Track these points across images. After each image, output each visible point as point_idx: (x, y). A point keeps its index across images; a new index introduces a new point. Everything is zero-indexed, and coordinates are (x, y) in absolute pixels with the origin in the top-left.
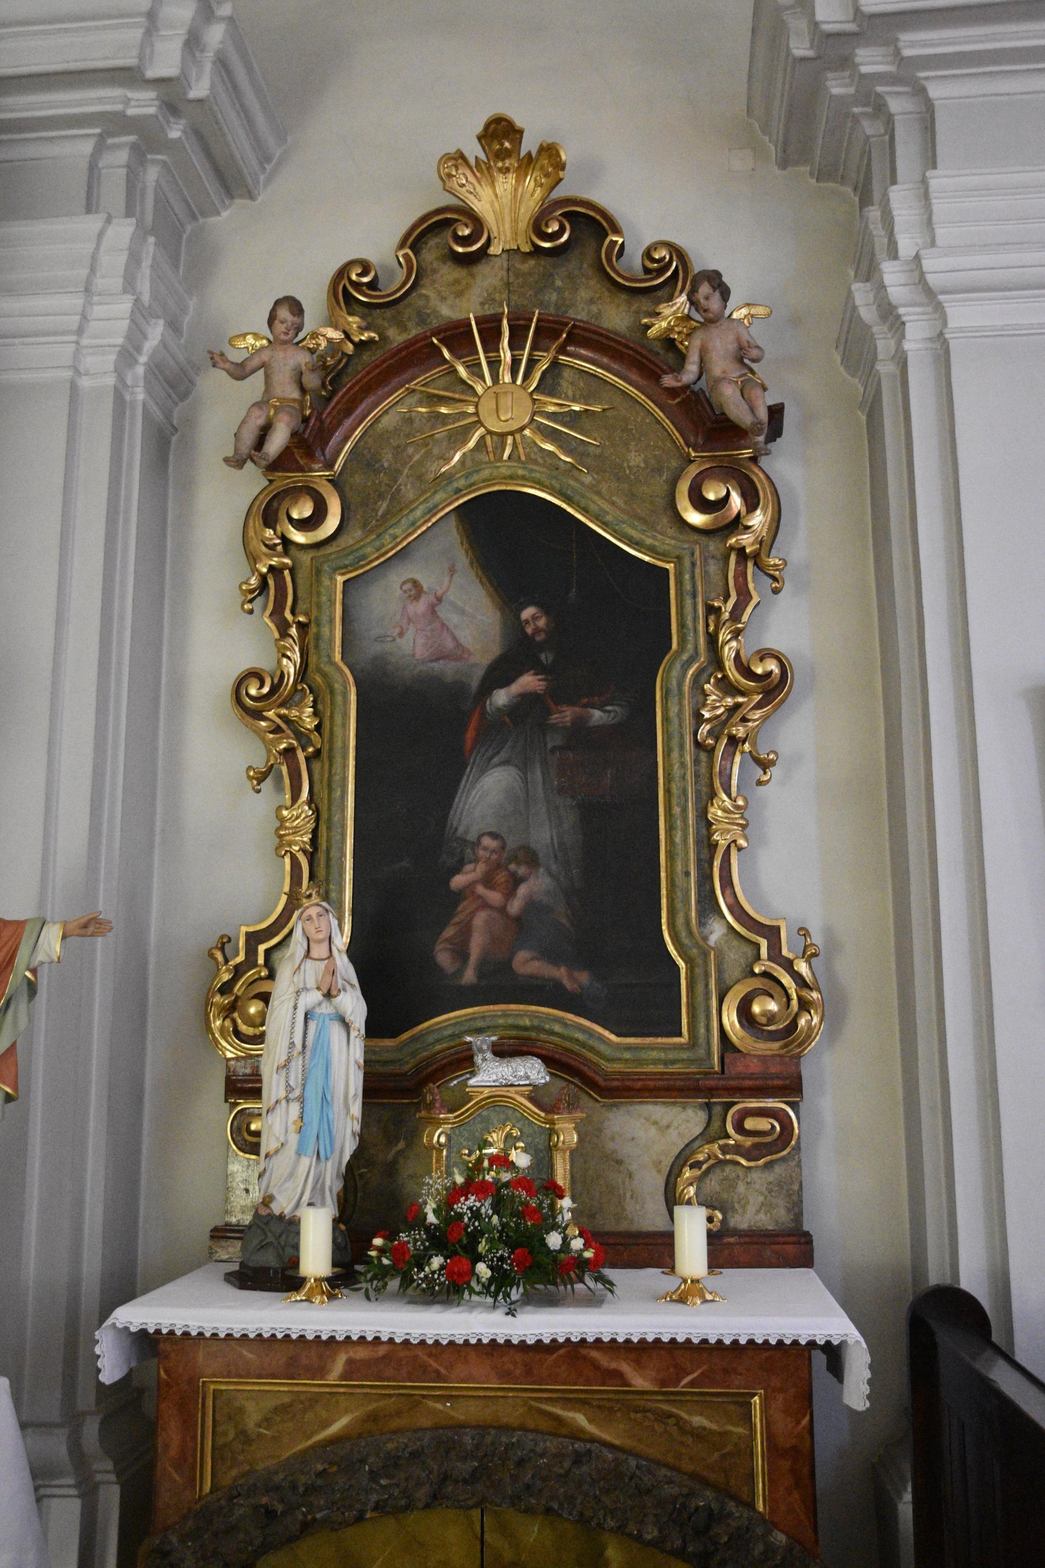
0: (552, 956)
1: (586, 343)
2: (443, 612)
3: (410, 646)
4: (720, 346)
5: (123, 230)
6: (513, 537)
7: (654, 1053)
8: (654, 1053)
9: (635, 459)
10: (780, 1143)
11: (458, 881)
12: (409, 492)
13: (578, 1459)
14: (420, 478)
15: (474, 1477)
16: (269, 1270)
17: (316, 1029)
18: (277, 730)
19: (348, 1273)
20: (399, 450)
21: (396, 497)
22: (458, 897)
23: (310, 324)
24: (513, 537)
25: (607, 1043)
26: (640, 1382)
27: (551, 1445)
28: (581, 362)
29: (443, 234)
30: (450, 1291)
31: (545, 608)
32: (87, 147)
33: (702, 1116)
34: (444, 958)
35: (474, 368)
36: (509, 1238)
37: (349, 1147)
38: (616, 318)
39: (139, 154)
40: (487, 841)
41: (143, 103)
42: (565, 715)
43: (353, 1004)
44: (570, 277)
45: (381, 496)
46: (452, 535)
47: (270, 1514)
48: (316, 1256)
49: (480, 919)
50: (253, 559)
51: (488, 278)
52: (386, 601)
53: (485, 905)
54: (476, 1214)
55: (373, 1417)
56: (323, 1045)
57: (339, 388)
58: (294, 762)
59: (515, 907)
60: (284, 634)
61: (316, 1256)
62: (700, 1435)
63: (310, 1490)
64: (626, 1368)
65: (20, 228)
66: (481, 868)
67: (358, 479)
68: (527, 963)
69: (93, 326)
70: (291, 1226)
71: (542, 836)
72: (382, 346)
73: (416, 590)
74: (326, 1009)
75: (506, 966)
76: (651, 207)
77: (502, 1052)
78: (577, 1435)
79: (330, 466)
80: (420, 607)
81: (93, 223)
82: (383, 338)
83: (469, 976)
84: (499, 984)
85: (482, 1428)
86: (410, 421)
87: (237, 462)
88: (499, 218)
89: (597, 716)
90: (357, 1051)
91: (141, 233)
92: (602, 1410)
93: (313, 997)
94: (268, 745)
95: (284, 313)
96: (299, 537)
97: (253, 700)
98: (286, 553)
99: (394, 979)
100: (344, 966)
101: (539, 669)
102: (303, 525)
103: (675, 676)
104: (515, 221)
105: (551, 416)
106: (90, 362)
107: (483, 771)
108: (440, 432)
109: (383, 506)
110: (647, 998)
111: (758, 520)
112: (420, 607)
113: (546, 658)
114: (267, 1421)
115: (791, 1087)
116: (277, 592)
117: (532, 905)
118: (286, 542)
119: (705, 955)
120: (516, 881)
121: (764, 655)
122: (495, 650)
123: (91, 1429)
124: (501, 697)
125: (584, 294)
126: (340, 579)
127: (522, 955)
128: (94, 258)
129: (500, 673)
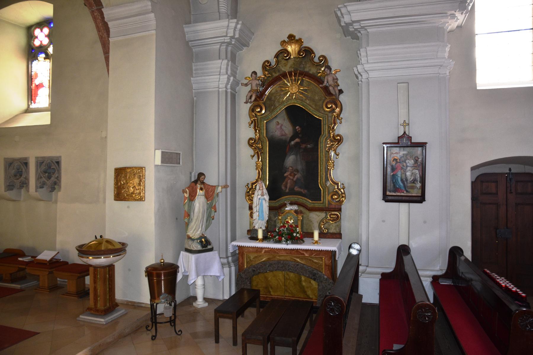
0: (300, 187)
1: (308, 76)
2: (283, 127)
3: (277, 134)
4: (330, 79)
5: (225, 62)
6: (295, 113)
7: (317, 204)
8: (317, 204)
9: (317, 98)
10: (337, 219)
11: (285, 175)
12: (277, 105)
14: (279, 102)
15: (282, 267)
16: (254, 238)
17: (262, 200)
18: (255, 149)
19: (265, 238)
20: (275, 97)
21: (275, 106)
22: (286, 177)
23: (259, 75)
24: (295, 113)
25: (309, 202)
26: (307, 255)
27: (293, 263)
28: (306, 79)
29: (282, 54)
30: (279, 241)
31: (300, 127)
32: (219, 46)
33: (325, 214)
34: (283, 188)
36: (288, 234)
37: (267, 218)
38: (313, 71)
39: (227, 46)
40: (290, 168)
41: (227, 40)
42: (303, 146)
43: (267, 197)
44: (305, 62)
45: (272, 105)
47: (254, 271)
48: (260, 235)
49: (289, 181)
50: (250, 118)
51: (291, 63)
52: (273, 126)
53: (290, 179)
54: (283, 230)
55: (269, 259)
56: (262, 204)
58: (259, 153)
59: (295, 179)
60: (256, 132)
61: (260, 235)
62: (316, 263)
63: (260, 268)
64: (305, 253)
66: (289, 172)
67: (268, 102)
68: (297, 189)
69: (221, 80)
70: (256, 231)
71: (299, 167)
72: (272, 75)
73: (278, 123)
74: (262, 197)
75: (293, 189)
76: (320, 49)
78: (298, 262)
79: (263, 100)
80: (279, 126)
81: (220, 61)
82: (272, 75)
83: (287, 191)
84: (292, 192)
85: (284, 261)
86: (277, 91)
87: (246, 103)
90: (267, 204)
91: (228, 61)
92: (301, 259)
94: (254, 151)
95: (253, 75)
96: (258, 114)
97: (252, 143)
98: (256, 117)
99: (274, 192)
100: (265, 191)
101: (299, 138)
103: (322, 139)
104: (295, 51)
105: (301, 90)
106: (221, 86)
107: (290, 156)
108: (282, 93)
109: (272, 107)
110: (316, 195)
111: (338, 110)
112: (279, 126)
113: (300, 136)
114: (254, 258)
115: (340, 210)
116: (256, 124)
117: (297, 179)
119: (325, 188)
120: (295, 175)
121: (338, 135)
123: (230, 259)
124: (293, 143)
125: (308, 65)
127: (296, 187)
128: (221, 67)
129: (292, 138)
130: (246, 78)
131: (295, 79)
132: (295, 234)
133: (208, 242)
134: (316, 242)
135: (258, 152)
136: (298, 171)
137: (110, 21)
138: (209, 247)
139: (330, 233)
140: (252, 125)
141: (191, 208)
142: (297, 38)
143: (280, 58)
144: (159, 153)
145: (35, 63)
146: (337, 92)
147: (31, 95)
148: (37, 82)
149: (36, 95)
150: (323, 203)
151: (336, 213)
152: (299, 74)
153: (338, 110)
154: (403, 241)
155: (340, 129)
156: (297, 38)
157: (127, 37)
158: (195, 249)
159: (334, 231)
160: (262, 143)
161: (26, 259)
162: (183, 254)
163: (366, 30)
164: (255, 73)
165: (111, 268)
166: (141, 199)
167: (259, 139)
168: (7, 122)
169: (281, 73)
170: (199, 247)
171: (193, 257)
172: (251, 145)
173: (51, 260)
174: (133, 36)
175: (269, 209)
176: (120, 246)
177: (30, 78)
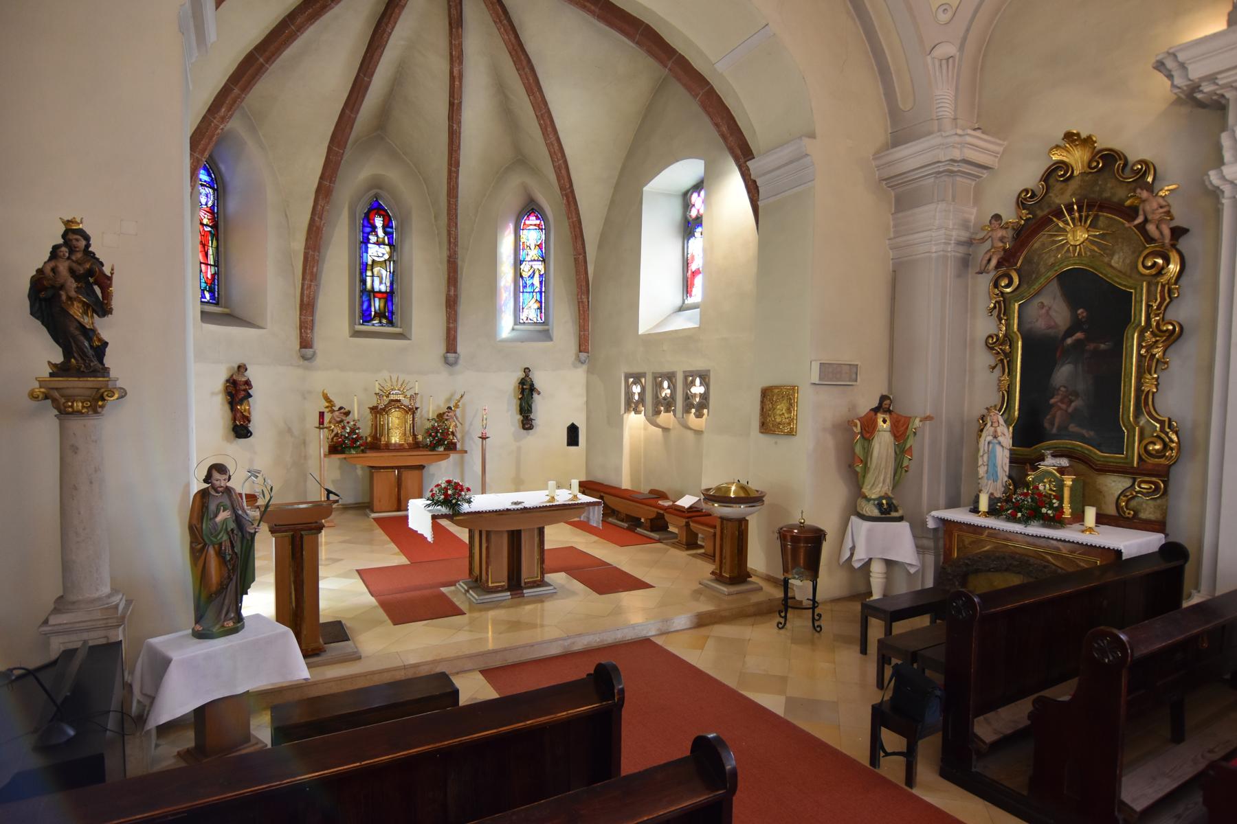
3: (1040, 325)
6: (1080, 285)
11: (1052, 401)
13: (1045, 567)
16: (975, 510)
17: (999, 444)
19: (993, 512)
22: (1052, 406)
29: (1055, 173)
34: (1046, 425)
35: (1067, 223)
42: (1091, 346)
46: (1054, 287)
49: (1059, 413)
51: (1074, 185)
52: (1033, 310)
57: (1024, 235)
59: (1070, 410)
61: (984, 505)
65: (917, 210)
71: (1081, 387)
72: (1037, 215)
73: (1042, 305)
77: (1054, 456)
78: (1048, 561)
82: (1035, 216)
83: (1054, 431)
88: (1077, 162)
89: (1102, 346)
90: (1007, 453)
93: (990, 438)
99: (1030, 434)
101: (1083, 331)
102: (1007, 286)
107: (1062, 365)
113: (1085, 327)
117: (1075, 409)
118: (1002, 293)
120: (1071, 401)
122: (1068, 325)
124: (1069, 341)
126: (1017, 305)
129: (1069, 332)
130: (983, 229)
131: (1081, 217)
132: (1044, 510)
133: (892, 507)
134: (1090, 530)
135: (1002, 360)
136: (1076, 394)
137: (759, 177)
138: (894, 514)
139: (1140, 519)
140: (995, 313)
141: (868, 451)
142: (1084, 135)
143: (1051, 181)
144: (816, 367)
145: (692, 241)
146: (1167, 232)
147: (687, 287)
148: (693, 267)
149: (692, 284)
150: (1126, 457)
151: (1154, 479)
152: (1092, 207)
153: (1174, 268)
154: (244, 361)
155: (1184, 311)
156: (1084, 135)
157: (778, 197)
158: (869, 514)
159: (1152, 517)
160: (1012, 345)
161: (667, 504)
162: (854, 519)
163: (695, 273)
164: (997, 217)
165: (742, 523)
166: (791, 433)
167: (1005, 335)
168: (658, 326)
169: (1054, 207)
170: (876, 513)
171: (866, 525)
172: (990, 348)
173: (691, 507)
174: (787, 194)
175: (1011, 462)
176: (757, 495)
177: (686, 263)
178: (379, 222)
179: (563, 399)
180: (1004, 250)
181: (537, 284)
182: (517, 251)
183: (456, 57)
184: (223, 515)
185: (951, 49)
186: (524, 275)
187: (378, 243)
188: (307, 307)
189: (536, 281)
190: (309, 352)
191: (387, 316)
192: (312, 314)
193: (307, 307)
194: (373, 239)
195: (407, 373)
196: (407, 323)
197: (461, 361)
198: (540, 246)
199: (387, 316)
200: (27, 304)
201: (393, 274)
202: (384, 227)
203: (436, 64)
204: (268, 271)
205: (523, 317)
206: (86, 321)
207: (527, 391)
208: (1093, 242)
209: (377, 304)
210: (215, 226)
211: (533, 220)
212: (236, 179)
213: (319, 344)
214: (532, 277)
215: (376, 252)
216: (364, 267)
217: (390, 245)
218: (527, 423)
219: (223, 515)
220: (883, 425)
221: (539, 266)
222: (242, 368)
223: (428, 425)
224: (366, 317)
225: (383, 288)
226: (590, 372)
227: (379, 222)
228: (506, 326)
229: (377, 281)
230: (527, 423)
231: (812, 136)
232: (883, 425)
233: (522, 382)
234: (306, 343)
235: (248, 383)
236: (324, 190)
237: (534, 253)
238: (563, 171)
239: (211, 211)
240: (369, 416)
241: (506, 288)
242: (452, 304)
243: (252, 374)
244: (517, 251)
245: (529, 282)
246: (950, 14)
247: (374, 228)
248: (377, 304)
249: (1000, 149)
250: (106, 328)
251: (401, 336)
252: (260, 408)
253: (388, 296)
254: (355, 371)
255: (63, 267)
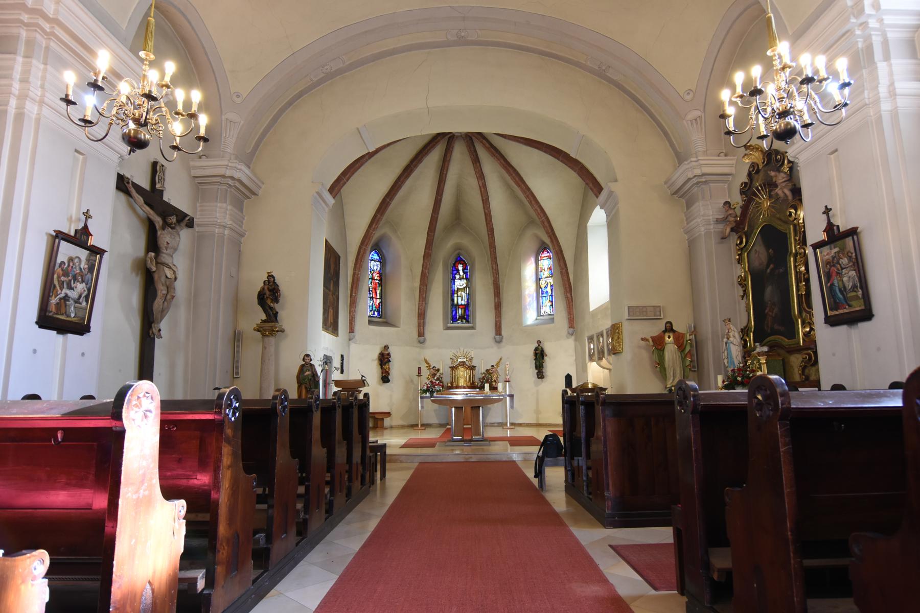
178: (460, 267)
179: (562, 362)
180: (736, 221)
181: (550, 291)
182: (533, 274)
183: (481, 176)
184: (307, 373)
185: (697, 113)
186: (543, 286)
187: (460, 279)
188: (422, 315)
189: (549, 289)
190: (422, 339)
191: (466, 318)
192: (424, 318)
193: (422, 315)
194: (457, 277)
195: (477, 347)
196: (474, 322)
197: (504, 340)
198: (550, 269)
199: (466, 318)
200: (256, 300)
201: (468, 295)
202: (463, 270)
203: (472, 182)
204: (404, 303)
205: (542, 312)
206: (272, 305)
207: (540, 355)
208: (773, 207)
209: (460, 311)
210: (381, 280)
211: (545, 254)
212: (389, 257)
213: (428, 335)
214: (546, 287)
215: (459, 283)
216: (453, 292)
217: (467, 279)
218: (540, 375)
219: (307, 373)
220: (669, 340)
221: (550, 280)
222: (386, 347)
223: (481, 376)
224: (454, 319)
225: (463, 303)
226: (576, 340)
227: (460, 267)
228: (530, 317)
229: (460, 299)
230: (540, 375)
231: (616, 181)
232: (669, 340)
233: (536, 349)
234: (421, 334)
235: (389, 354)
236: (428, 255)
237: (547, 273)
238: (546, 223)
239: (379, 273)
240: (449, 370)
241: (530, 296)
242: (498, 307)
243: (393, 351)
244: (533, 274)
245: (545, 291)
246: (691, 94)
247: (458, 271)
248: (460, 311)
249: (734, 162)
250: (277, 307)
251: (473, 328)
252: (396, 368)
253: (466, 307)
254: (445, 347)
255: (266, 288)
